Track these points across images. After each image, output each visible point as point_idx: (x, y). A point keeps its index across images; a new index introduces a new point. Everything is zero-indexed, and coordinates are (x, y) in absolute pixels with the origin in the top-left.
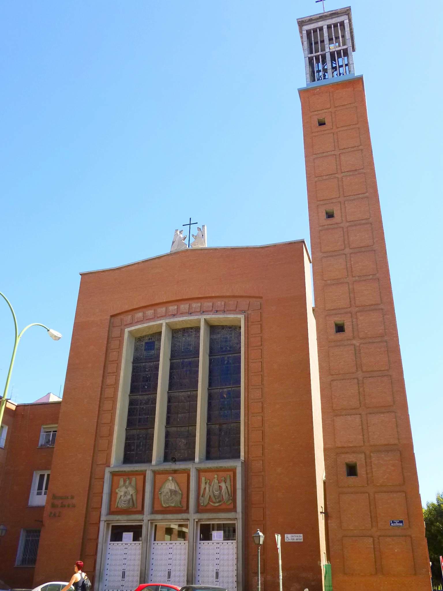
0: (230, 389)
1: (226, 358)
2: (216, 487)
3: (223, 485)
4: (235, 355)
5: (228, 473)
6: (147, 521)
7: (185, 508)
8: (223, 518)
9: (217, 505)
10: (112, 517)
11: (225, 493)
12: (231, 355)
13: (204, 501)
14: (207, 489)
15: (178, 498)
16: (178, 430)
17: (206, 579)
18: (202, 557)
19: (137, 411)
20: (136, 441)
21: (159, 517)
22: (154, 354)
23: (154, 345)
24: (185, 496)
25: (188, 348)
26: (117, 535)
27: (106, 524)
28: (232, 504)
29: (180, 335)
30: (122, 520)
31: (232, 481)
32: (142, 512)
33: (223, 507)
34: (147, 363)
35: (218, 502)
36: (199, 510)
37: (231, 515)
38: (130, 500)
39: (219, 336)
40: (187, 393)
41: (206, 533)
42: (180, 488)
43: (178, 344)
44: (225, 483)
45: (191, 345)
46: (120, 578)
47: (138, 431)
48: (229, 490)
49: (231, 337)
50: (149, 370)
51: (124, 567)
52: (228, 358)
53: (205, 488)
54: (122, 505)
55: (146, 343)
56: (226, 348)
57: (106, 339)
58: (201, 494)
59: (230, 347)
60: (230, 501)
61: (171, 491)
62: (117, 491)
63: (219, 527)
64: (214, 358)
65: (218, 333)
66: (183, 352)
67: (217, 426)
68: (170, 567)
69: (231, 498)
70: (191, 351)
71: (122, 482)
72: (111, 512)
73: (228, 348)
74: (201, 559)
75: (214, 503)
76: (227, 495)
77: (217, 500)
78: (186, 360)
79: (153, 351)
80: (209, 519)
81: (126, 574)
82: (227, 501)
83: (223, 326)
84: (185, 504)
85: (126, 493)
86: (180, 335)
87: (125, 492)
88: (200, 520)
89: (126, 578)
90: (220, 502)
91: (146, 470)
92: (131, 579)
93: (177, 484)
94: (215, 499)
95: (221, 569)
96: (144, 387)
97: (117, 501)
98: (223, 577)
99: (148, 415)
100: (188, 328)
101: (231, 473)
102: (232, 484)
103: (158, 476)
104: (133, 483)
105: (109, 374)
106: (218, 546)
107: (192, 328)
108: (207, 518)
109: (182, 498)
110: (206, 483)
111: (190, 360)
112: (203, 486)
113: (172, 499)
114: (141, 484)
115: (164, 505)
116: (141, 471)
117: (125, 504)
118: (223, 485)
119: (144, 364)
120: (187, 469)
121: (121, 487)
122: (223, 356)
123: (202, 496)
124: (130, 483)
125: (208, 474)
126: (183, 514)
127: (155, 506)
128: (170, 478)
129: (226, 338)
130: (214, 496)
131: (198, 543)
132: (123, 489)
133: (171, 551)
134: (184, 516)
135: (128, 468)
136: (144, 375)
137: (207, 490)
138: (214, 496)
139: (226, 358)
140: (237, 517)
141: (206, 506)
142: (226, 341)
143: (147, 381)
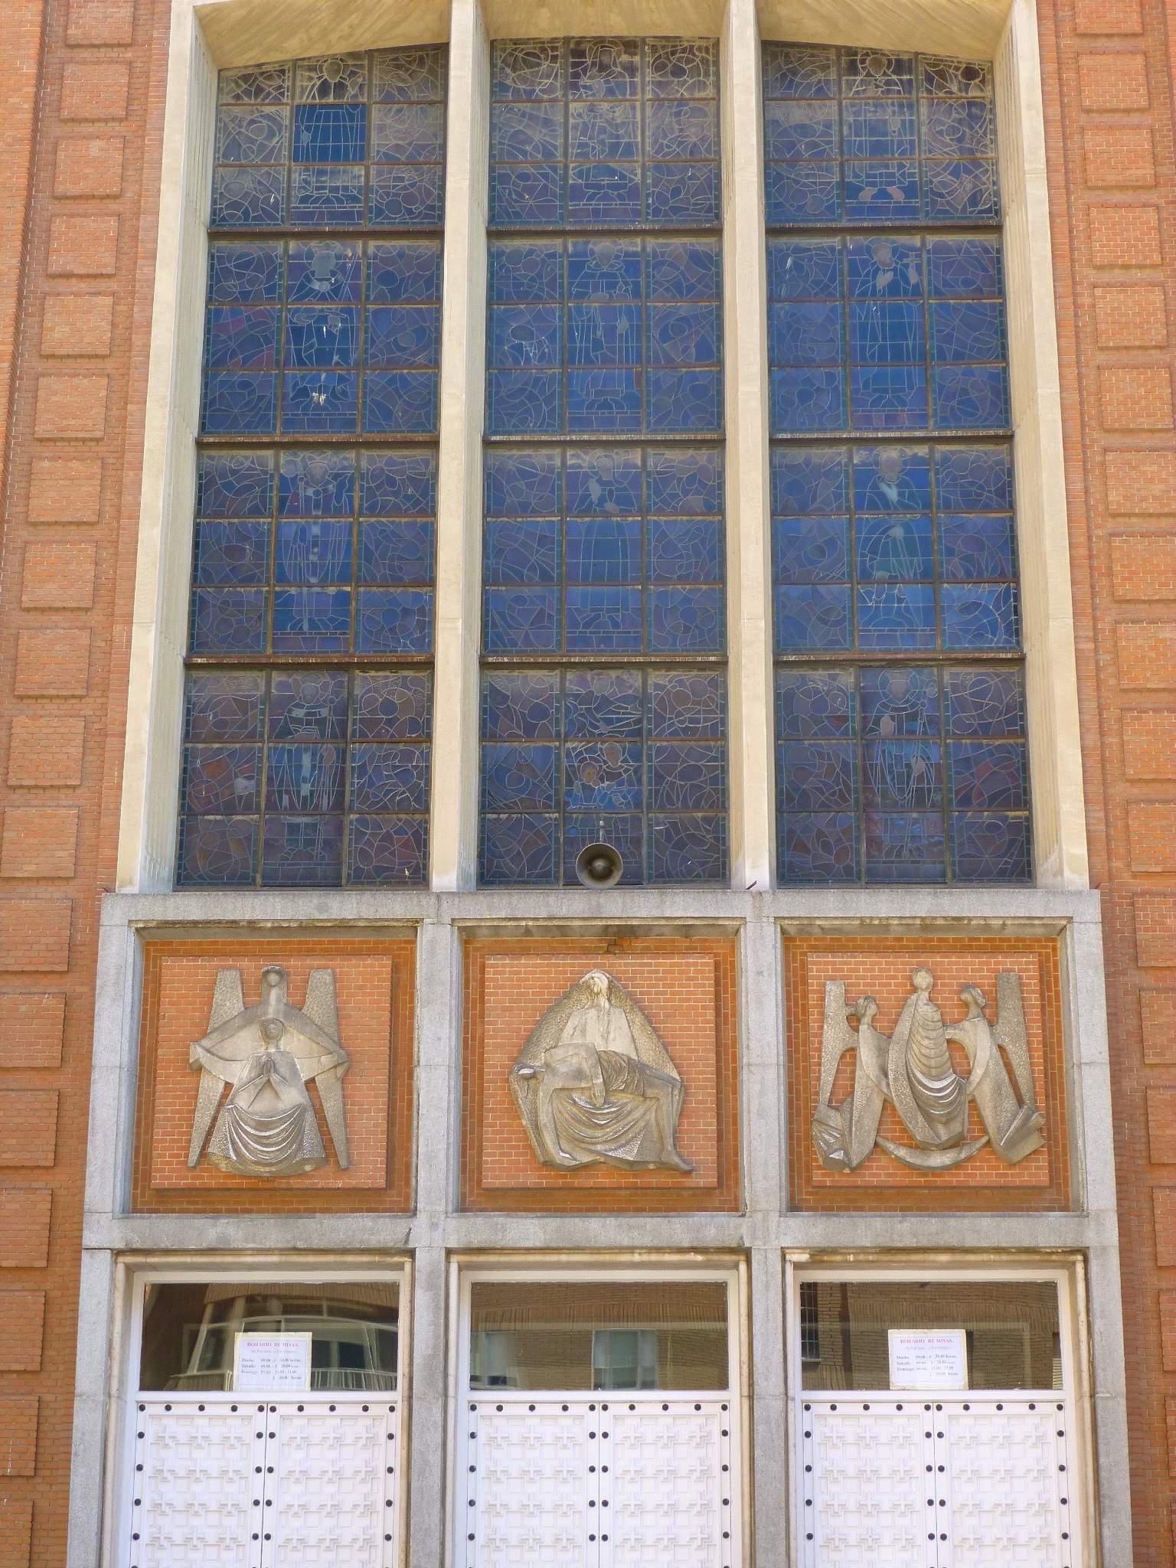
0: (922, 451)
1: (884, 255)
2: (927, 1046)
4: (950, 239)
5: (1007, 962)
8: (981, 1246)
9: (938, 1160)
10: (165, 1229)
11: (998, 1089)
12: (916, 240)
13: (848, 1135)
14: (867, 1057)
16: (572, 687)
19: (259, 546)
22: (367, 189)
23: (363, 133)
24: (704, 1096)
25: (612, 172)
26: (184, 1339)
27: (121, 1268)
28: (1043, 1161)
29: (548, 78)
30: (245, 1250)
32: (394, 1192)
33: (983, 1175)
34: (314, 244)
35: (945, 1147)
37: (1047, 1229)
38: (300, 1110)
39: (827, 111)
40: (620, 456)
41: (842, 1340)
43: (538, 135)
45: (629, 150)
47: (277, 677)
48: (1022, 1073)
49: (911, 127)
50: (336, 290)
52: (899, 253)
53: (850, 1055)
54: (245, 1148)
55: (304, 114)
56: (883, 194)
57: (33, 51)
59: (910, 191)
60: (1034, 1142)
61: (610, 1066)
63: (927, 1306)
64: (797, 250)
65: (821, 93)
66: (576, 193)
67: (847, 679)
69: (1037, 1119)
70: (634, 192)
71: (229, 1001)
72: (146, 1195)
73: (897, 194)
74: (818, 1504)
75: (923, 1148)
76: (1010, 1104)
77: (944, 1134)
78: (602, 246)
79: (359, 170)
80: (890, 1253)
82: (1012, 1144)
83: (851, 52)
84: (704, 1155)
85: (266, 1069)
86: (548, 78)
87: (258, 1070)
88: (820, 1256)
91: (414, 926)
93: (649, 1019)
94: (929, 1119)
96: (304, 392)
97: (202, 1120)
99: (344, 579)
100: (601, 43)
101: (1025, 966)
103: (500, 969)
104: (318, 1004)
105: (61, 285)
106: (936, 1421)
107: (630, 45)
108: (868, 1246)
110: (854, 1020)
111: (635, 244)
112: (833, 1037)
113: (617, 1117)
115: (562, 1157)
116: (378, 928)
118: (978, 1040)
119: (293, 245)
120: (713, 925)
121: (226, 1029)
122: (862, 240)
124: (296, 1007)
125: (866, 967)
126: (699, 1218)
127: (490, 1158)
128: (600, 981)
129: (877, 128)
130: (922, 1105)
132: (246, 1045)
134: (713, 1227)
135: (194, 906)
136: (304, 322)
138: (922, 1105)
139: (884, 255)
140: (1090, 1238)
142: (879, 149)
143: (323, 358)
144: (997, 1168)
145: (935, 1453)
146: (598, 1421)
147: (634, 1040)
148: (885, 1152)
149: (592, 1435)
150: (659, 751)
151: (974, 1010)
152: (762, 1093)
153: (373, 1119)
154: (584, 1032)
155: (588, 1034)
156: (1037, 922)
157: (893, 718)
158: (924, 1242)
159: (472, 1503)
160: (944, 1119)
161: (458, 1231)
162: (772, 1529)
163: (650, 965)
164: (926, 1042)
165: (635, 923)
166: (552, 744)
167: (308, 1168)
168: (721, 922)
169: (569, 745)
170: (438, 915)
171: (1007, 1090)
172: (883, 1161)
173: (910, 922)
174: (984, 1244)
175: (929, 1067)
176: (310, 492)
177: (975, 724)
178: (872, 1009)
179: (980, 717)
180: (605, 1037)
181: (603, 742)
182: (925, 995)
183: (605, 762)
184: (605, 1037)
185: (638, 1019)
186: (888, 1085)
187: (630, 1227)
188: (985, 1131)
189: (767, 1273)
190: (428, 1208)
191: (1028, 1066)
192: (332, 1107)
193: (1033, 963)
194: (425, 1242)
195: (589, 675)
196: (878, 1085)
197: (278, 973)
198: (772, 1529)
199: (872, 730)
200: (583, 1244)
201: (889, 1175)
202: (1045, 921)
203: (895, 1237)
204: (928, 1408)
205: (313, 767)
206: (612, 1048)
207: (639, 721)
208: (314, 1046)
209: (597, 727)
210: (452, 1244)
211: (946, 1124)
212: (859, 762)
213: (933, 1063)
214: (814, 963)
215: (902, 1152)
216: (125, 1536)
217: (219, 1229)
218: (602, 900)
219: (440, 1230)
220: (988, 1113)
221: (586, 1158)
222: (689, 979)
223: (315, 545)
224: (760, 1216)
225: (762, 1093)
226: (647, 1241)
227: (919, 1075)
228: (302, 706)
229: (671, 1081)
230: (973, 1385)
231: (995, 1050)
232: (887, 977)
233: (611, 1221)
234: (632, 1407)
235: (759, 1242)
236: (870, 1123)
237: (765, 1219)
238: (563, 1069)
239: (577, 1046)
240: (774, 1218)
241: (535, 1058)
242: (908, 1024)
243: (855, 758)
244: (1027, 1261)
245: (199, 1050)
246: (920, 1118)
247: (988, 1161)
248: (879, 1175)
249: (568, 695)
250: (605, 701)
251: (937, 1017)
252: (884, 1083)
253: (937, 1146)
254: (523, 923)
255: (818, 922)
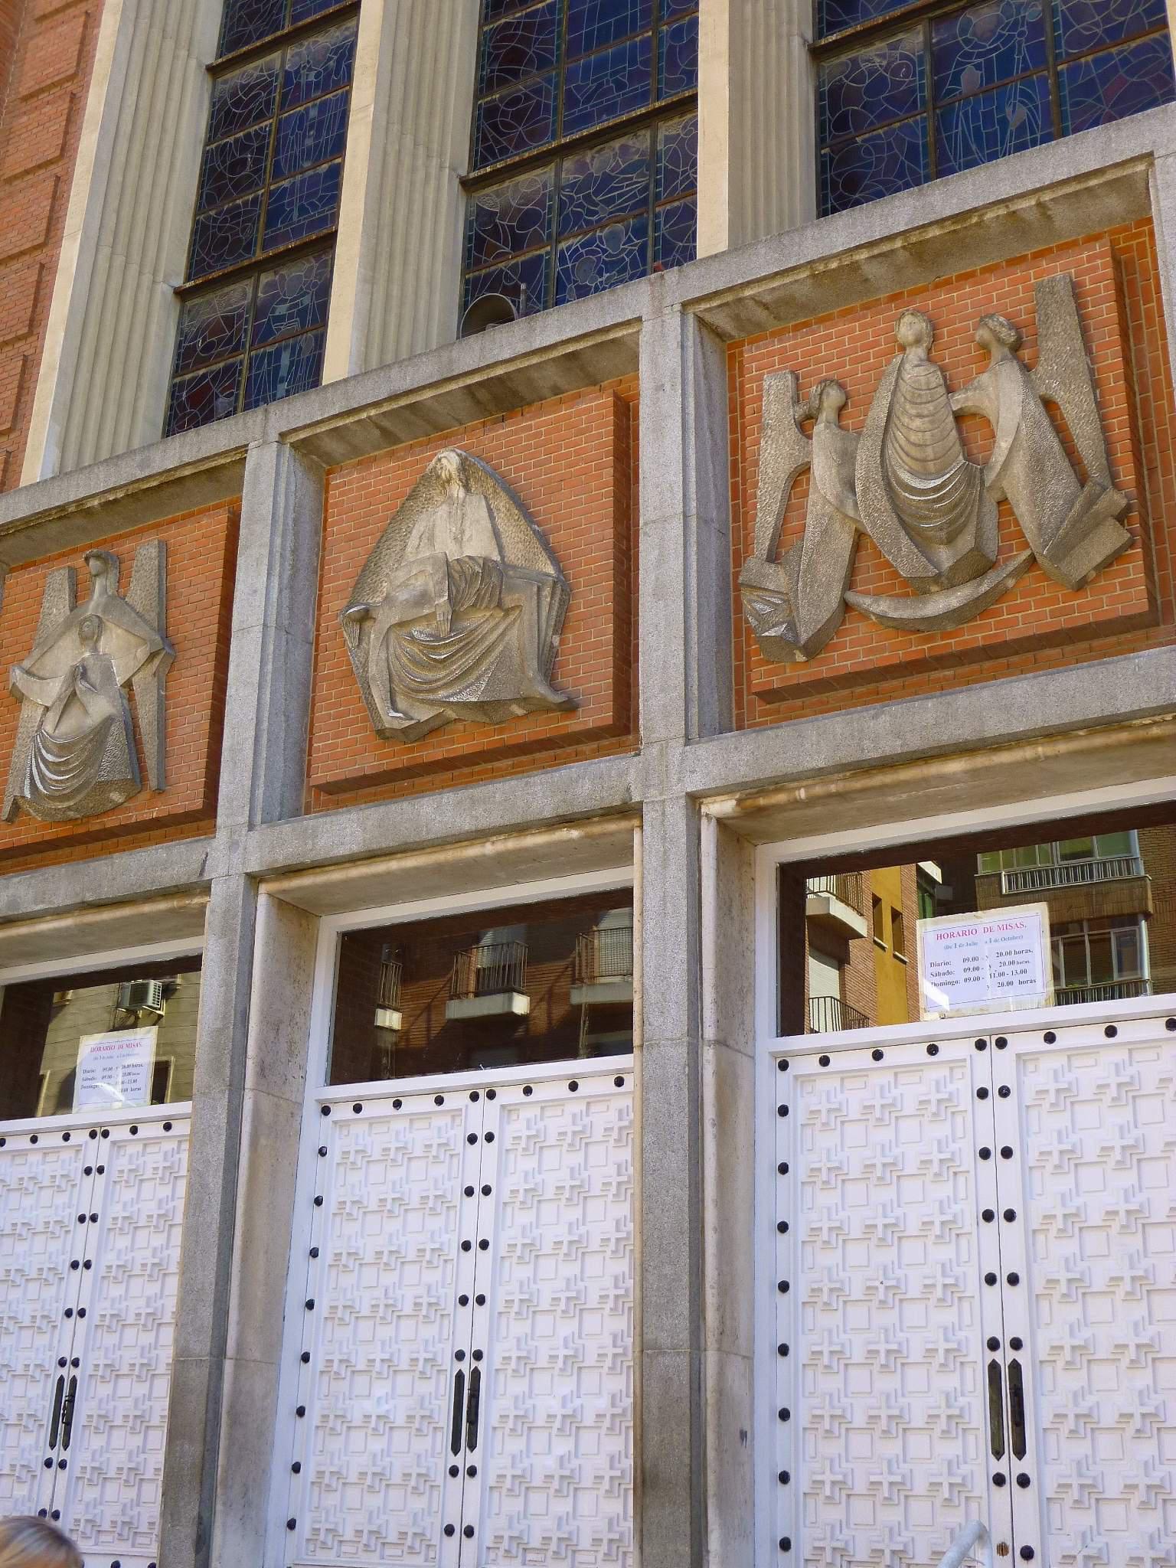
2: (920, 429)
3: (1004, 398)
6: (239, 884)
7: (598, 713)
11: (1037, 465)
13: (798, 594)
15: (514, 633)
17: (354, 1423)
18: (812, 1208)
20: (244, 357)
21: (345, 830)
24: (596, 596)
28: (1134, 569)
31: (1107, 336)
35: (948, 581)
36: (749, 684)
42: (543, 539)
44: (1027, 368)
46: (34, 1443)
51: (71, 1339)
53: (801, 474)
58: (762, 541)
60: (1109, 538)
62: (17, 676)
68: (471, 1329)
75: (918, 588)
76: (1061, 484)
77: (946, 557)
81: (83, 1409)
82: (1064, 548)
84: (590, 677)
89: (496, 1449)
90: (978, 566)
91: (244, 449)
92: (546, 1457)
95: (1046, 1334)
98: (1086, 1423)
102: (1111, 358)
106: (996, 1068)
109: (561, 626)
110: (805, 425)
112: (773, 456)
114: (198, 587)
117: (54, 767)
118: (1004, 398)
123: (773, 557)
124: (119, 597)
131: (765, 1066)
132: (67, 654)
133: (481, 1164)
134: (588, 781)
137: (822, 479)
141: (814, 649)
144: (1054, 600)
145: (997, 1123)
146: (483, 1116)
147: (496, 534)
148: (864, 615)
149: (490, 1137)
150: (669, 215)
151: (997, 352)
152: (661, 560)
153: (193, 724)
154: (431, 539)
155: (438, 540)
156: (1093, 183)
157: (978, 67)
158: (915, 743)
159: (314, 1253)
160: (943, 534)
161: (259, 850)
162: (668, 1270)
163: (530, 428)
164: (917, 423)
165: (500, 371)
166: (542, 251)
167: (116, 797)
168: (612, 336)
169: (563, 245)
170: (265, 433)
171: (1057, 459)
172: (862, 629)
173: (885, 248)
174: (1019, 727)
175: (924, 461)
176: (312, 78)
177: (1099, 31)
178: (834, 397)
179: (1107, 19)
180: (458, 540)
181: (602, 228)
182: (916, 353)
183: (604, 251)
184: (458, 540)
185: (502, 503)
186: (856, 504)
187: (473, 801)
188: (1026, 545)
189: (664, 839)
190: (229, 822)
191: (1094, 416)
192: (146, 715)
193: (1101, 256)
194: (222, 870)
195: (588, 156)
196: (839, 508)
197: (98, 557)
198: (668, 1270)
199: (950, 92)
200: (413, 838)
201: (871, 651)
202: (1110, 176)
203: (867, 743)
204: (981, 1045)
205: (292, 363)
206: (469, 551)
207: (646, 188)
208: (132, 639)
209: (593, 213)
210: (254, 867)
211: (950, 541)
212: (930, 139)
213: (930, 452)
214: (754, 359)
215: (883, 606)
216: (764, 1287)
217: (11, 891)
218: (454, 354)
219: (241, 850)
220: (1023, 509)
221: (423, 714)
222: (582, 432)
223: (311, 127)
224: (655, 750)
225: (661, 560)
226: (496, 819)
227: (905, 477)
228: (284, 301)
229: (540, 580)
230: (1063, 998)
231: (1036, 409)
232: (864, 348)
233: (449, 798)
234: (528, 1091)
235: (653, 792)
236: (831, 570)
237: (662, 753)
238: (403, 596)
239: (422, 561)
240: (677, 748)
241: (374, 591)
242: (885, 403)
243: (924, 136)
244: (1107, 748)
245: (18, 672)
246: (905, 540)
247: (1036, 592)
248: (855, 655)
249: (563, 188)
250: (607, 179)
251: (936, 379)
252: (850, 503)
253: (937, 579)
254: (364, 415)
255: (748, 293)
